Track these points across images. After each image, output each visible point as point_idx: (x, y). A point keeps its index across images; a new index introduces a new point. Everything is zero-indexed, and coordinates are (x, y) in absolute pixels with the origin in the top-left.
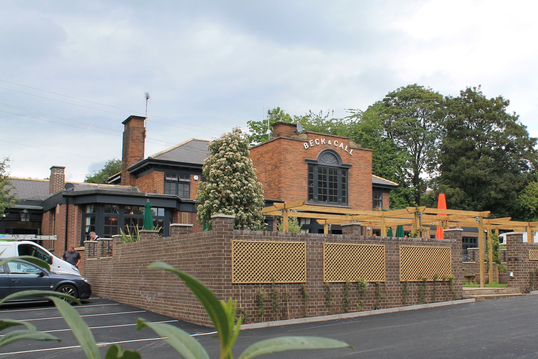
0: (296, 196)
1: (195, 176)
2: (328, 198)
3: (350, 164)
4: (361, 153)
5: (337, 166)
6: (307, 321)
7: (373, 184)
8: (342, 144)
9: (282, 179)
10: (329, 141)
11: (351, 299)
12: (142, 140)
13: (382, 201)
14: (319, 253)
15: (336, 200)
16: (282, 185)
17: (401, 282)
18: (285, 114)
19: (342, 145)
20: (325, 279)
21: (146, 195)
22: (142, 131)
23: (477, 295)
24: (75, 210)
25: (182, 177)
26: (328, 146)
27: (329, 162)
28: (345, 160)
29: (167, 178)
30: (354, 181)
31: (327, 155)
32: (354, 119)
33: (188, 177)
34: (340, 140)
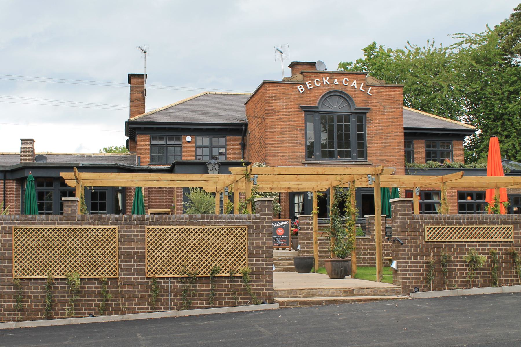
0: (288, 154)
1: (188, 137)
2: (336, 153)
3: (368, 107)
4: (386, 91)
5: (349, 111)
6: (472, 294)
7: (405, 129)
8: (355, 81)
9: (268, 133)
10: (336, 80)
11: (59, 301)
12: (142, 100)
13: (452, 151)
14: (6, 241)
15: (348, 155)
16: (267, 141)
17: (148, 278)
18: (386, 51)
19: (355, 83)
20: (14, 273)
22: (141, 90)
23: (304, 297)
24: (12, 186)
25: (171, 139)
26: (334, 86)
27: (336, 106)
28: (359, 103)
29: (154, 142)
30: (374, 129)
31: (333, 98)
32: (466, 46)
33: (179, 139)
34: (353, 77)
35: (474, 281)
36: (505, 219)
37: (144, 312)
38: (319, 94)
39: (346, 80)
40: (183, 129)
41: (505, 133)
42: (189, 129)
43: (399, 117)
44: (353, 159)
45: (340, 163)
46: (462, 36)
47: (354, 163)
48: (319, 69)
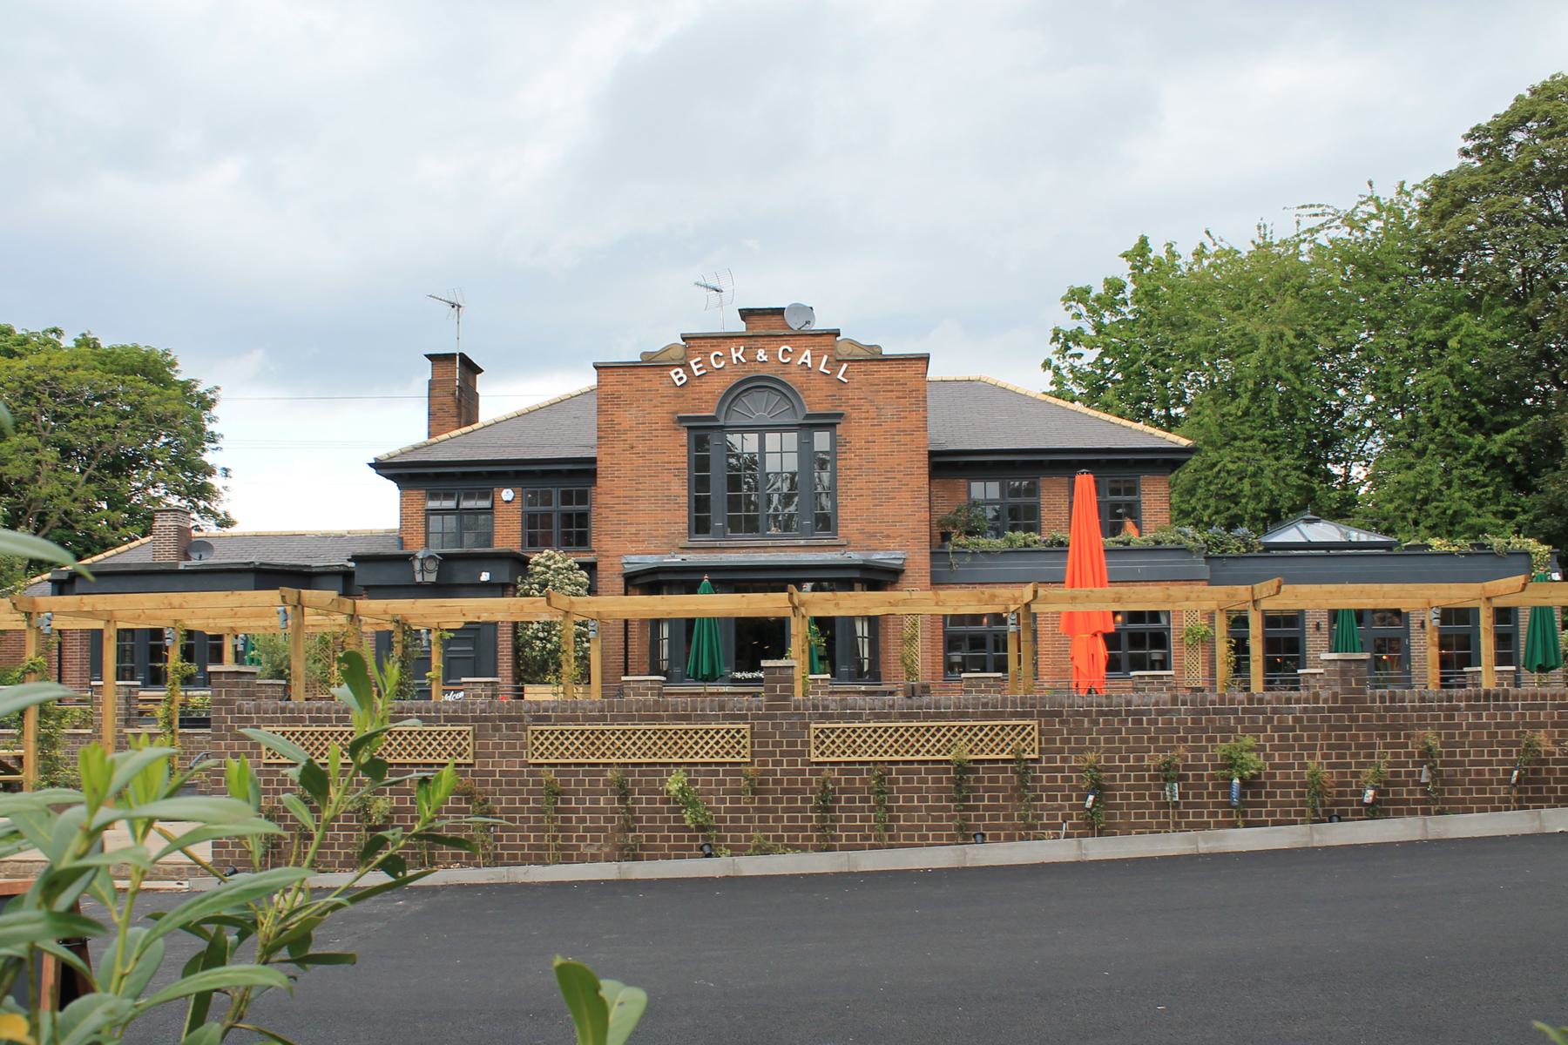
0: (647, 527)
6: (522, 879)
7: (932, 454)
8: (808, 352)
10: (761, 352)
21: (181, 567)
25: (469, 497)
31: (756, 395)
35: (1166, 815)
36: (455, 711)
37: (683, 857)
38: (719, 385)
39: (785, 350)
40: (492, 475)
41: (1416, 445)
42: (505, 473)
43: (918, 429)
44: (803, 535)
45: (770, 543)
46: (1319, 211)
47: (802, 542)
48: (795, 323)
